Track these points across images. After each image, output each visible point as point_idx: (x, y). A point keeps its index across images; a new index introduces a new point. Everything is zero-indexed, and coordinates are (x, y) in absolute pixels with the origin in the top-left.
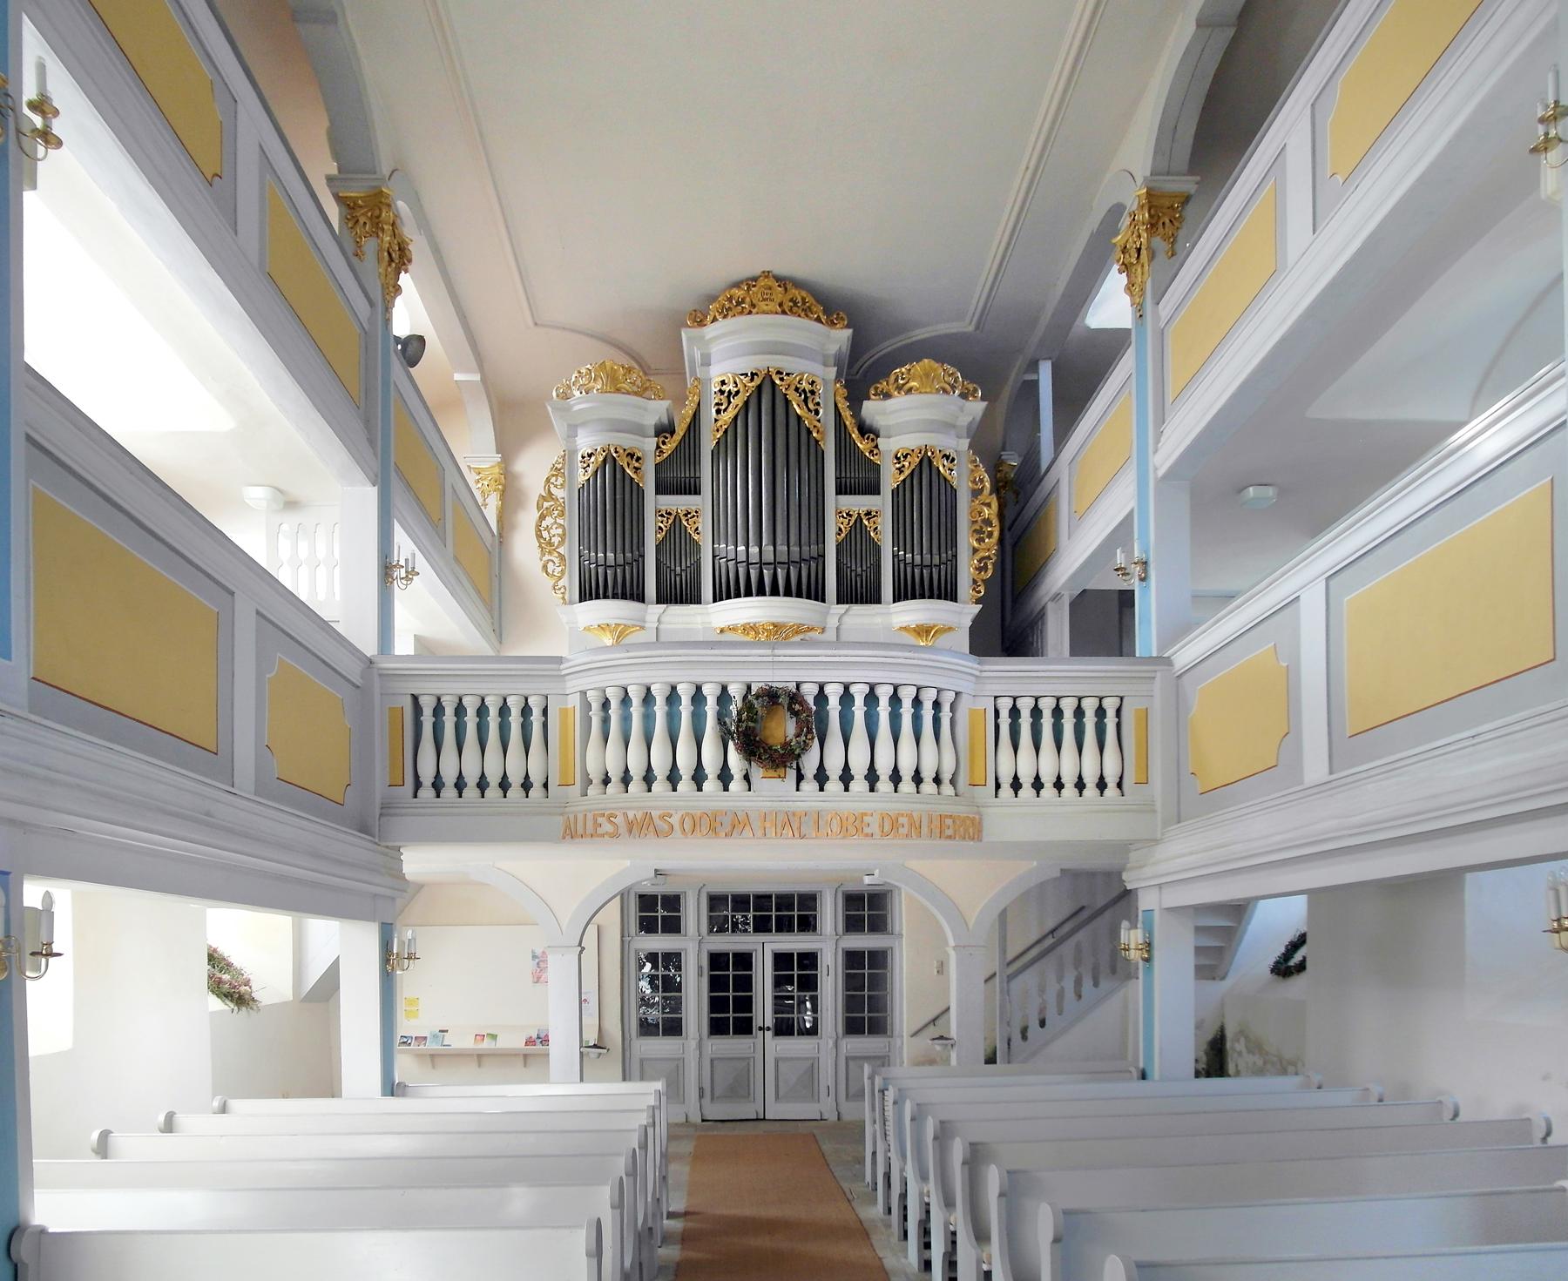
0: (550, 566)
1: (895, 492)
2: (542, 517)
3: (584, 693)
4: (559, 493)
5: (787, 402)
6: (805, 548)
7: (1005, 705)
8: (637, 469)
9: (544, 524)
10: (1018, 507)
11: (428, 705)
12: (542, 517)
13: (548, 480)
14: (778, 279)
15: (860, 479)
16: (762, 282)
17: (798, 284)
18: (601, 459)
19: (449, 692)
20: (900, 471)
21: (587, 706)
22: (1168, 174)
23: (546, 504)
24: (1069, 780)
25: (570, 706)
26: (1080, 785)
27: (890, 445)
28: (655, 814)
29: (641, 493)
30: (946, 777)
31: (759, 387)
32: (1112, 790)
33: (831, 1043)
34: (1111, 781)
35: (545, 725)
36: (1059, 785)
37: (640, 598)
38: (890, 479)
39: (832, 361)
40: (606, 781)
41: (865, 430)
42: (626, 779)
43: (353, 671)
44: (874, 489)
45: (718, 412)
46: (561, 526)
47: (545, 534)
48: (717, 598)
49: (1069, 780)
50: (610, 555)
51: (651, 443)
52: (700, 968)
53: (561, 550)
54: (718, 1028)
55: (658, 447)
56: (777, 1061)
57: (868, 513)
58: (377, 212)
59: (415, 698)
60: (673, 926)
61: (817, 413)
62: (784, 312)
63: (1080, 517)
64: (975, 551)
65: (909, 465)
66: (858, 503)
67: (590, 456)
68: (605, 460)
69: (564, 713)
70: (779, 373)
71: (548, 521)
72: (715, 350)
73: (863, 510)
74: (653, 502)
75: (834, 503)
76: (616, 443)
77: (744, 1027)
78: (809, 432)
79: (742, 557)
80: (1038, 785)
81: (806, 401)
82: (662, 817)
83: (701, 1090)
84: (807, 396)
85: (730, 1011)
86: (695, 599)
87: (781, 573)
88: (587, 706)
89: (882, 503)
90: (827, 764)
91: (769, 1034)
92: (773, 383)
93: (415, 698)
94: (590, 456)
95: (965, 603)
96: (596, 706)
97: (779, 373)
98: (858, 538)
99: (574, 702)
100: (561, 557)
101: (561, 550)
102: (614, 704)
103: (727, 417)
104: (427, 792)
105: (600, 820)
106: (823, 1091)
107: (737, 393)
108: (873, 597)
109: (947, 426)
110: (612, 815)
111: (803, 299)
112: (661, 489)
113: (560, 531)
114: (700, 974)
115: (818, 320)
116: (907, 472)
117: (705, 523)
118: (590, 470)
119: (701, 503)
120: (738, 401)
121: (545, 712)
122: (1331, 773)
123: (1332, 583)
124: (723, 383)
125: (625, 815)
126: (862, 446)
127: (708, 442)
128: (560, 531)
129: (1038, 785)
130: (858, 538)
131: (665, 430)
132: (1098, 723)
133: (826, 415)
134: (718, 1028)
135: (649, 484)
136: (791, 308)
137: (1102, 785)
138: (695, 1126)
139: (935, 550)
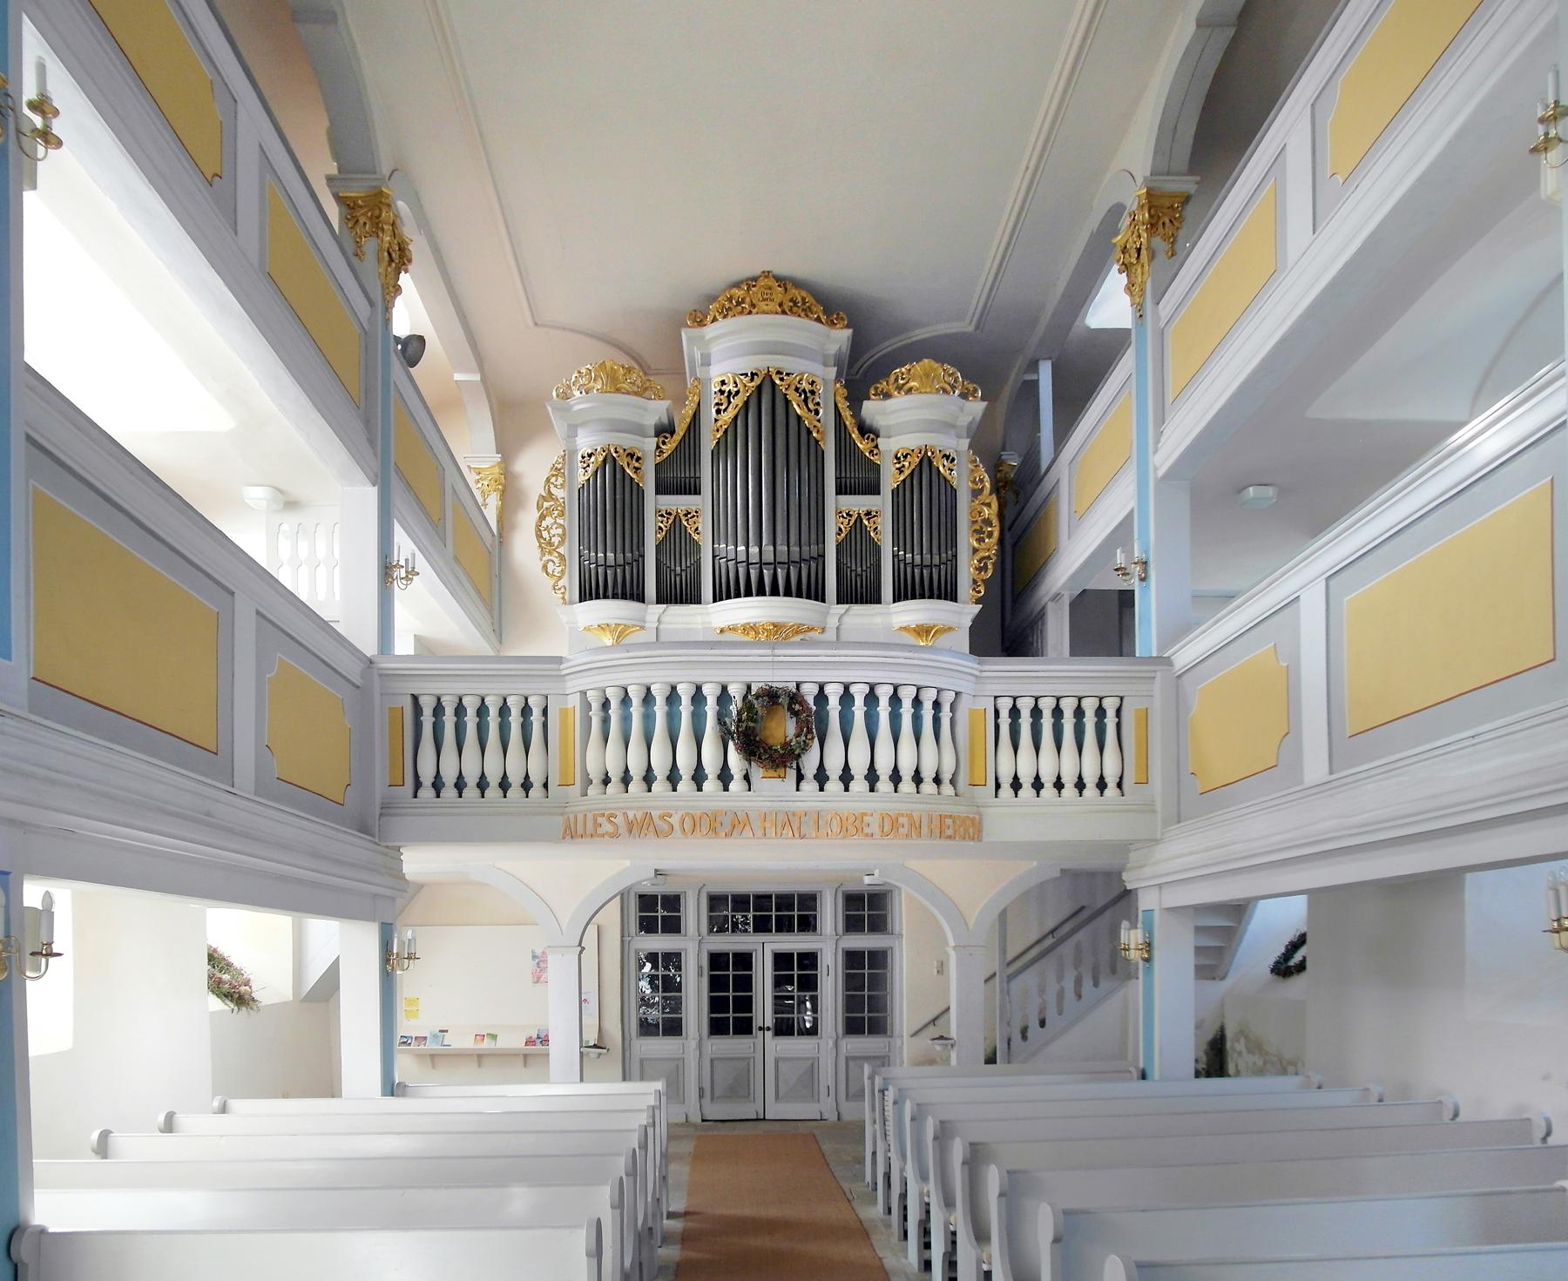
0: (550, 566)
1: (895, 492)
2: (542, 517)
3: (584, 693)
4: (559, 493)
5: (787, 402)
6: (805, 548)
7: (1005, 705)
8: (637, 469)
9: (544, 524)
10: (1018, 507)
11: (428, 705)
12: (542, 517)
13: (548, 480)
14: (778, 279)
15: (860, 479)
16: (762, 282)
17: (798, 284)
18: (601, 459)
19: (449, 692)
20: (900, 471)
21: (587, 706)
22: (1168, 174)
23: (546, 504)
24: (1069, 780)
25: (570, 706)
26: (1080, 785)
27: (890, 445)
28: (655, 814)
29: (641, 493)
30: (946, 777)
31: (759, 387)
32: (1112, 790)
33: (831, 1043)
34: (1111, 781)
35: (545, 725)
36: (1059, 785)
37: (640, 598)
38: (890, 479)
39: (832, 361)
40: (606, 781)
41: (865, 430)
42: (626, 779)
43: (353, 671)
44: (874, 489)
45: (718, 412)
46: (561, 526)
47: (545, 534)
48: (717, 598)
49: (1069, 780)
50: (610, 555)
51: (651, 443)
52: (700, 968)
53: (561, 550)
54: (718, 1028)
55: (658, 447)
56: (777, 1061)
57: (868, 513)
58: (377, 212)
59: (415, 698)
60: (673, 926)
61: (817, 413)
62: (784, 312)
63: (1080, 517)
64: (975, 551)
65: (909, 465)
66: (858, 503)
67: (590, 456)
68: (605, 460)
69: (564, 713)
70: (779, 373)
71: (548, 521)
72: (715, 350)
73: (863, 510)
74: (653, 502)
75: (834, 503)
76: (616, 443)
77: (744, 1027)
78: (809, 432)
79: (742, 557)
80: (1038, 785)
81: (806, 401)
82: (662, 817)
83: (701, 1090)
84: (807, 396)
85: (730, 1011)
86: (695, 599)
87: (781, 573)
88: (587, 706)
89: (882, 503)
90: (827, 764)
91: (769, 1034)
92: (773, 383)
93: (415, 698)
94: (590, 456)
95: (965, 603)
96: (596, 706)
97: (779, 373)
98: (858, 538)
99: (574, 702)
100: (561, 557)
101: (561, 550)
102: (614, 704)
103: (727, 417)
104: (427, 792)
105: (600, 820)
106: (823, 1091)
107: (737, 393)
108: (873, 597)
109: (947, 426)
110: (612, 815)
111: (803, 299)
112: (661, 489)
113: (560, 531)
114: (700, 974)
115: (818, 320)
116: (907, 472)
117: (705, 523)
118: (590, 470)
119: (701, 503)
120: (738, 401)
121: (545, 712)
122: (1331, 773)
123: (1332, 583)
124: (723, 383)
125: (625, 815)
126: (862, 446)
127: (708, 442)
128: (560, 531)
129: (1038, 785)
130: (858, 538)
131: (665, 430)
132: (1098, 723)
133: (826, 415)
134: (718, 1028)
135: (649, 484)
136: (791, 308)
137: (1102, 785)
138: (695, 1126)
139: (935, 550)
